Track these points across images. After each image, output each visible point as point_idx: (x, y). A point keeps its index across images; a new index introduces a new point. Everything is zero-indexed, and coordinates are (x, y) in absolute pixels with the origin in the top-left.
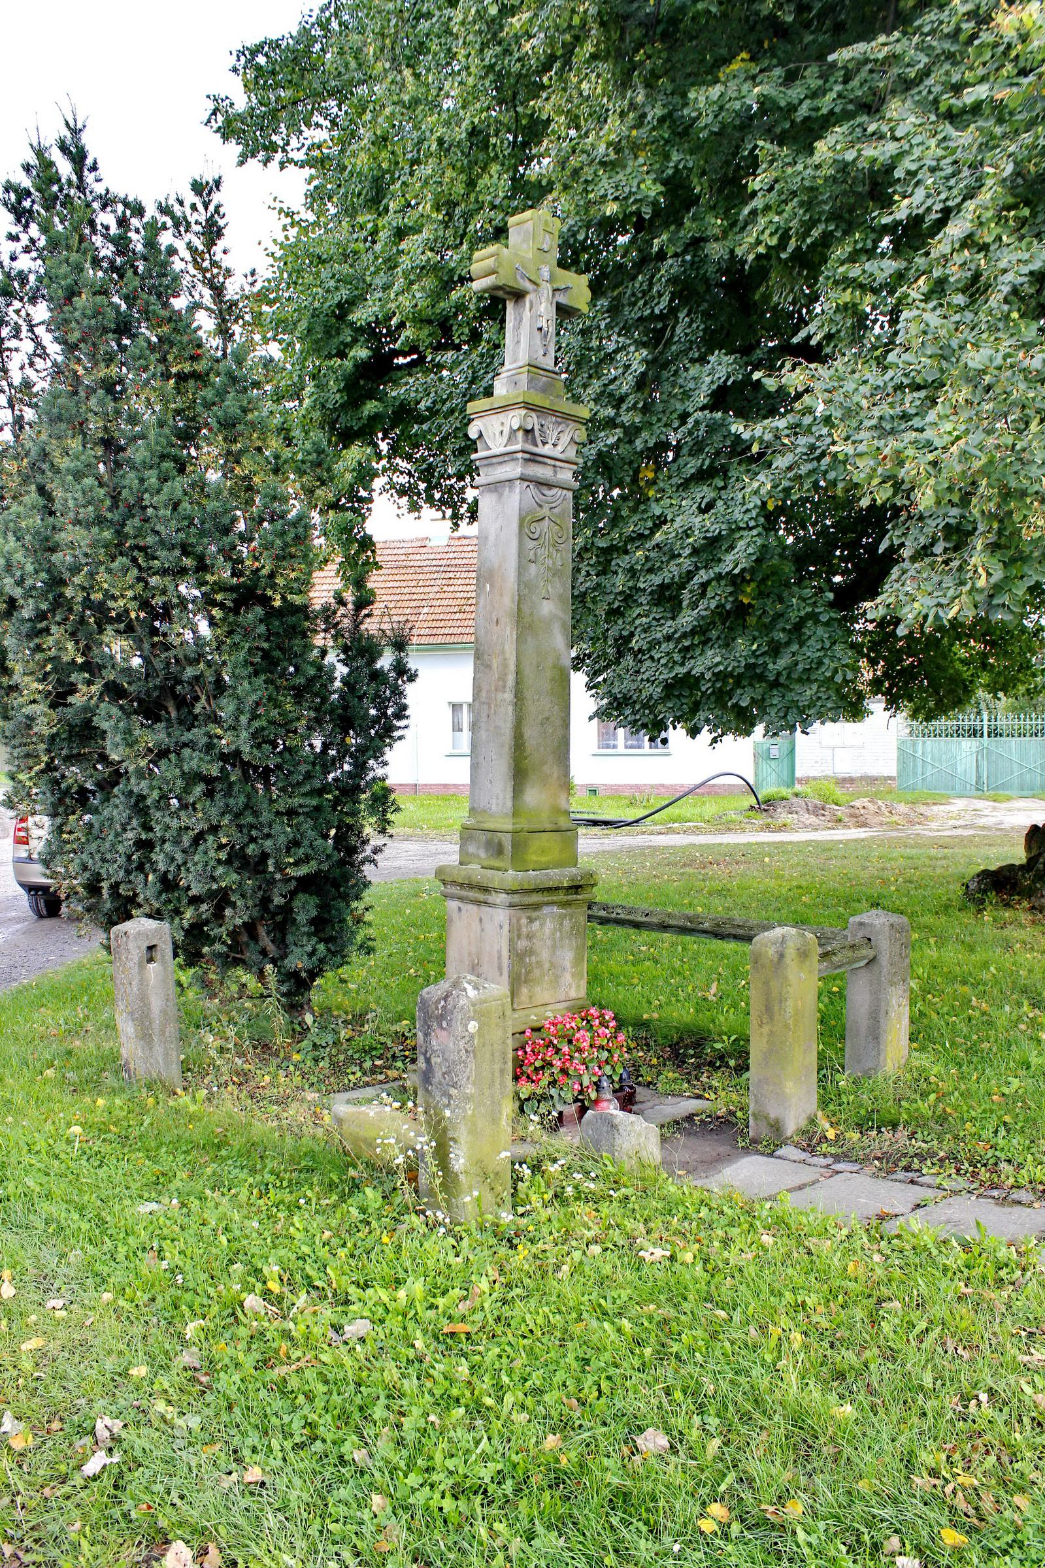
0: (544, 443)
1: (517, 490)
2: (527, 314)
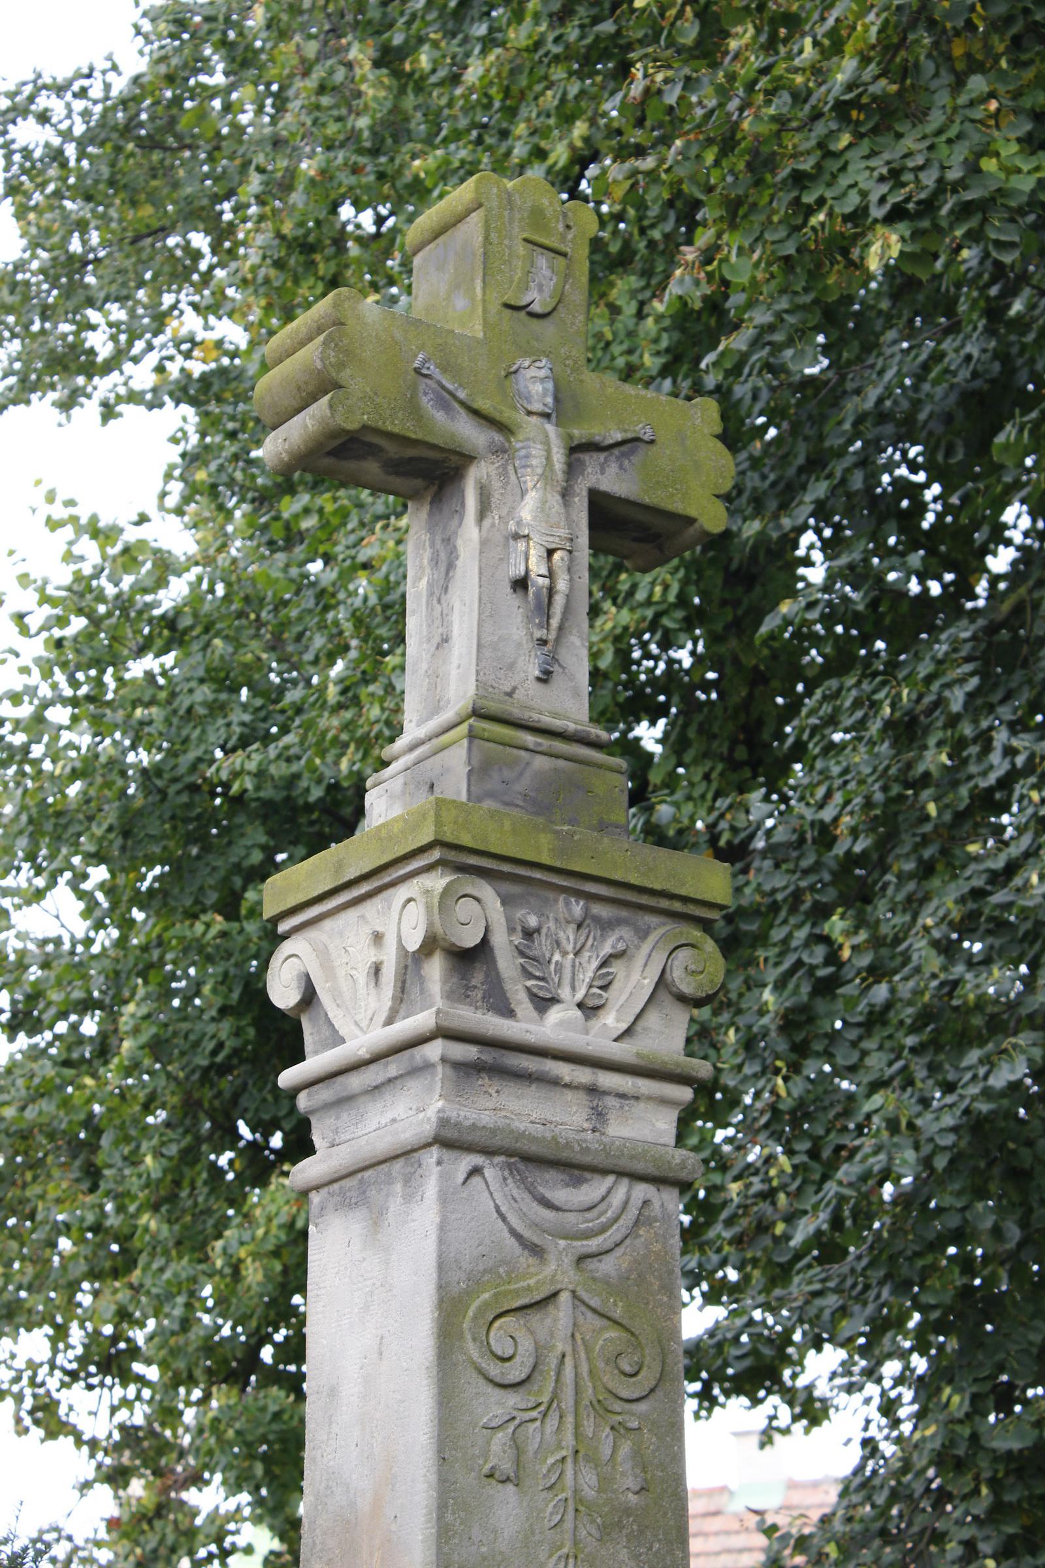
0: (543, 1003)
2: (469, 534)
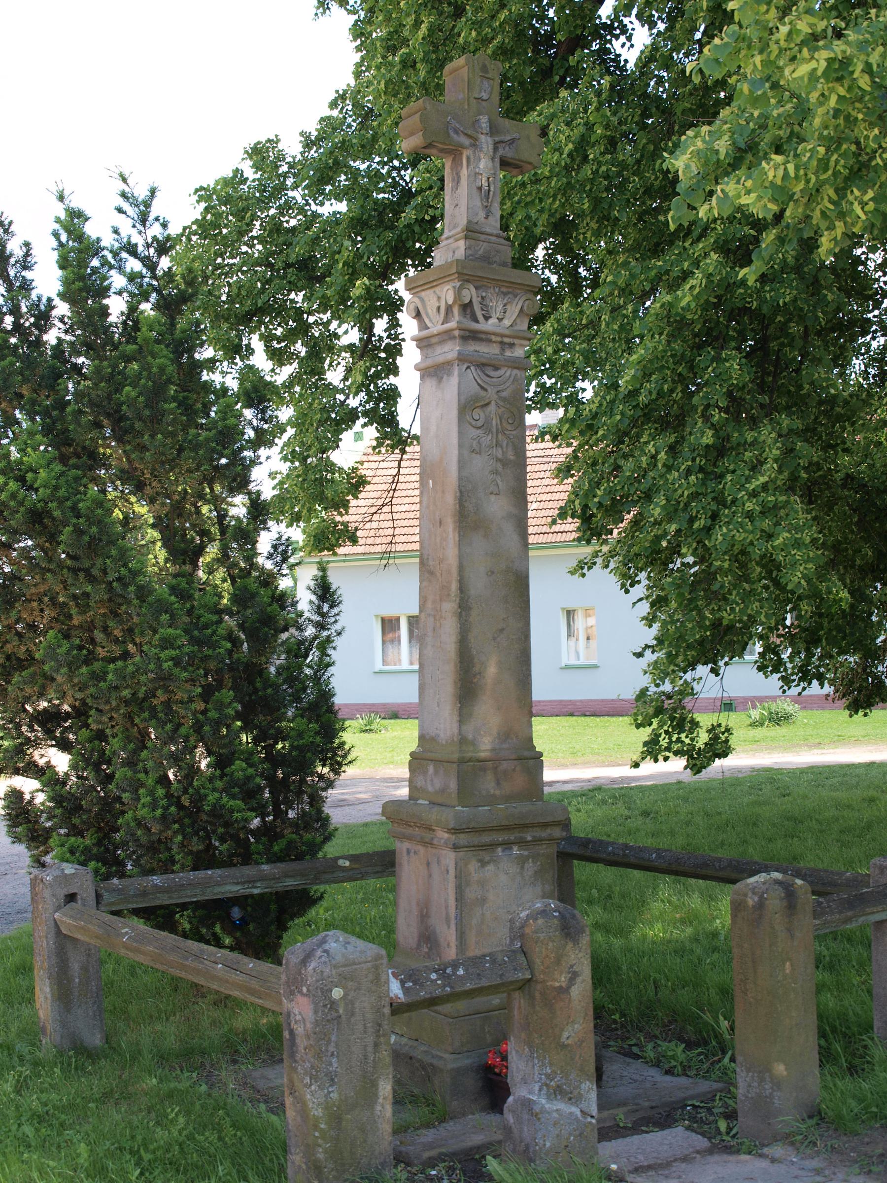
0: (487, 318)
1: (456, 373)
